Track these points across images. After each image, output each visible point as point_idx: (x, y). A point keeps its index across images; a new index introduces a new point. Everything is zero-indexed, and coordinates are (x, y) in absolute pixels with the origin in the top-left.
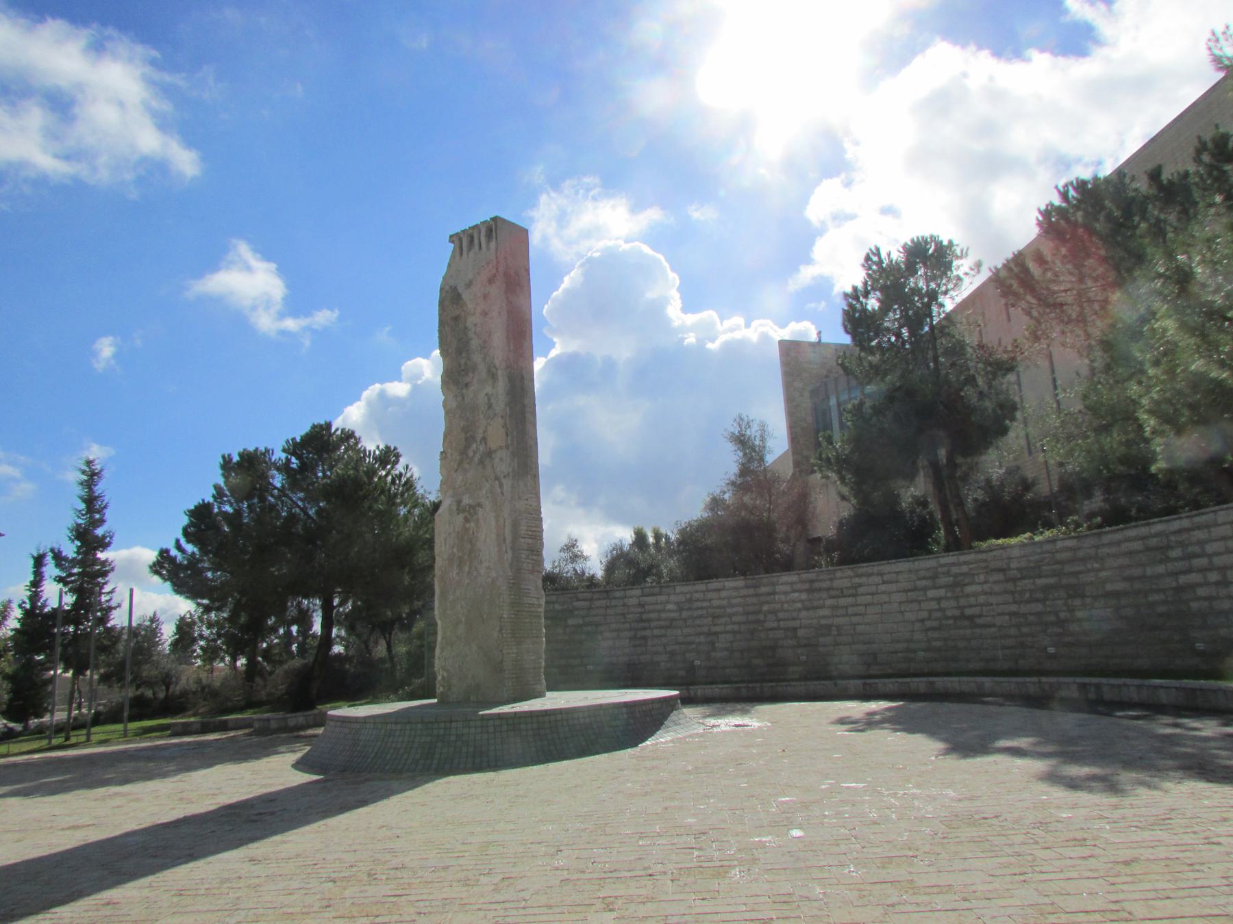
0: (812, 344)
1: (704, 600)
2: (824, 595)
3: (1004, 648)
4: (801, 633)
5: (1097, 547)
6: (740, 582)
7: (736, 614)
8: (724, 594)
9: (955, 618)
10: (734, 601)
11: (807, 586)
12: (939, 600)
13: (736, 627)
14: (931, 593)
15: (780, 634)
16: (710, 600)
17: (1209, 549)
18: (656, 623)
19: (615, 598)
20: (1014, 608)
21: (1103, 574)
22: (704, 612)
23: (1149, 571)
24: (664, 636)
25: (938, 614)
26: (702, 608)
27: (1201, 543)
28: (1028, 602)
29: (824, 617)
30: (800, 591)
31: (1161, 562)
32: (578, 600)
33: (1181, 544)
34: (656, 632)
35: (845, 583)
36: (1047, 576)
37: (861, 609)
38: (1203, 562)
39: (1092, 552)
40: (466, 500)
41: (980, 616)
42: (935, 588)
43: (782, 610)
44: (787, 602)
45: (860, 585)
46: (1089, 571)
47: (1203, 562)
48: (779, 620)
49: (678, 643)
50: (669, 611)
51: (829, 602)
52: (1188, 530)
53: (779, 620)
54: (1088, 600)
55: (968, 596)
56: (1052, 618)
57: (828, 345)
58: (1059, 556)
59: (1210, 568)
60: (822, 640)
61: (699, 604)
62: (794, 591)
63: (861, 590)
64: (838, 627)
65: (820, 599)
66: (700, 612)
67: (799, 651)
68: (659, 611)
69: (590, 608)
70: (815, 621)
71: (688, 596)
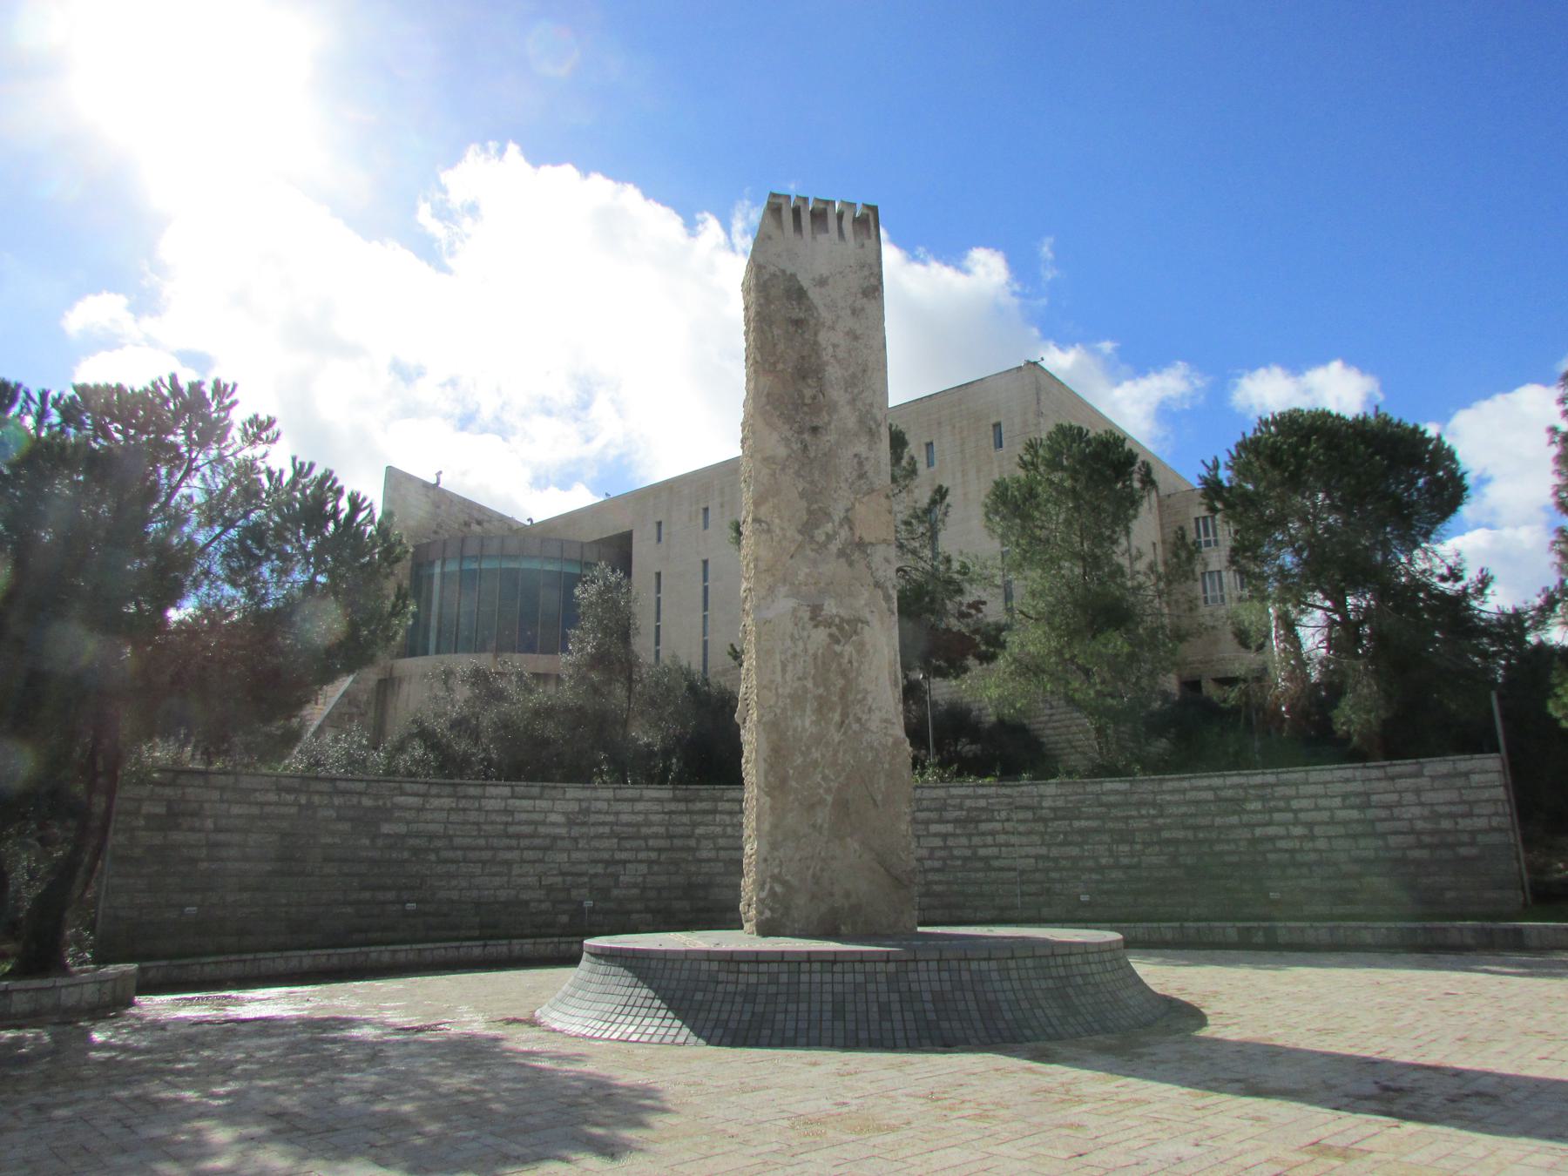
0: (426, 485)
1: (607, 813)
3: (1023, 894)
7: (656, 836)
8: (640, 806)
9: (965, 859)
10: (654, 818)
12: (945, 836)
13: (653, 855)
14: (934, 828)
16: (617, 813)
17: (1295, 804)
19: (465, 797)
20: (1043, 851)
21: (1160, 821)
22: (607, 830)
23: (1218, 821)
24: (541, 861)
25: (943, 853)
26: (603, 824)
27: (1287, 799)
28: (1062, 844)
31: (1234, 812)
32: (404, 793)
33: (1262, 798)
36: (1088, 819)
39: (1150, 797)
40: (830, 608)
41: (997, 858)
42: (941, 821)
46: (1142, 817)
48: (719, 849)
50: (553, 824)
52: (1273, 786)
54: (1138, 847)
55: (983, 834)
56: (1090, 863)
57: (444, 492)
58: (1104, 799)
59: (1296, 822)
61: (602, 818)
66: (601, 830)
71: (584, 805)
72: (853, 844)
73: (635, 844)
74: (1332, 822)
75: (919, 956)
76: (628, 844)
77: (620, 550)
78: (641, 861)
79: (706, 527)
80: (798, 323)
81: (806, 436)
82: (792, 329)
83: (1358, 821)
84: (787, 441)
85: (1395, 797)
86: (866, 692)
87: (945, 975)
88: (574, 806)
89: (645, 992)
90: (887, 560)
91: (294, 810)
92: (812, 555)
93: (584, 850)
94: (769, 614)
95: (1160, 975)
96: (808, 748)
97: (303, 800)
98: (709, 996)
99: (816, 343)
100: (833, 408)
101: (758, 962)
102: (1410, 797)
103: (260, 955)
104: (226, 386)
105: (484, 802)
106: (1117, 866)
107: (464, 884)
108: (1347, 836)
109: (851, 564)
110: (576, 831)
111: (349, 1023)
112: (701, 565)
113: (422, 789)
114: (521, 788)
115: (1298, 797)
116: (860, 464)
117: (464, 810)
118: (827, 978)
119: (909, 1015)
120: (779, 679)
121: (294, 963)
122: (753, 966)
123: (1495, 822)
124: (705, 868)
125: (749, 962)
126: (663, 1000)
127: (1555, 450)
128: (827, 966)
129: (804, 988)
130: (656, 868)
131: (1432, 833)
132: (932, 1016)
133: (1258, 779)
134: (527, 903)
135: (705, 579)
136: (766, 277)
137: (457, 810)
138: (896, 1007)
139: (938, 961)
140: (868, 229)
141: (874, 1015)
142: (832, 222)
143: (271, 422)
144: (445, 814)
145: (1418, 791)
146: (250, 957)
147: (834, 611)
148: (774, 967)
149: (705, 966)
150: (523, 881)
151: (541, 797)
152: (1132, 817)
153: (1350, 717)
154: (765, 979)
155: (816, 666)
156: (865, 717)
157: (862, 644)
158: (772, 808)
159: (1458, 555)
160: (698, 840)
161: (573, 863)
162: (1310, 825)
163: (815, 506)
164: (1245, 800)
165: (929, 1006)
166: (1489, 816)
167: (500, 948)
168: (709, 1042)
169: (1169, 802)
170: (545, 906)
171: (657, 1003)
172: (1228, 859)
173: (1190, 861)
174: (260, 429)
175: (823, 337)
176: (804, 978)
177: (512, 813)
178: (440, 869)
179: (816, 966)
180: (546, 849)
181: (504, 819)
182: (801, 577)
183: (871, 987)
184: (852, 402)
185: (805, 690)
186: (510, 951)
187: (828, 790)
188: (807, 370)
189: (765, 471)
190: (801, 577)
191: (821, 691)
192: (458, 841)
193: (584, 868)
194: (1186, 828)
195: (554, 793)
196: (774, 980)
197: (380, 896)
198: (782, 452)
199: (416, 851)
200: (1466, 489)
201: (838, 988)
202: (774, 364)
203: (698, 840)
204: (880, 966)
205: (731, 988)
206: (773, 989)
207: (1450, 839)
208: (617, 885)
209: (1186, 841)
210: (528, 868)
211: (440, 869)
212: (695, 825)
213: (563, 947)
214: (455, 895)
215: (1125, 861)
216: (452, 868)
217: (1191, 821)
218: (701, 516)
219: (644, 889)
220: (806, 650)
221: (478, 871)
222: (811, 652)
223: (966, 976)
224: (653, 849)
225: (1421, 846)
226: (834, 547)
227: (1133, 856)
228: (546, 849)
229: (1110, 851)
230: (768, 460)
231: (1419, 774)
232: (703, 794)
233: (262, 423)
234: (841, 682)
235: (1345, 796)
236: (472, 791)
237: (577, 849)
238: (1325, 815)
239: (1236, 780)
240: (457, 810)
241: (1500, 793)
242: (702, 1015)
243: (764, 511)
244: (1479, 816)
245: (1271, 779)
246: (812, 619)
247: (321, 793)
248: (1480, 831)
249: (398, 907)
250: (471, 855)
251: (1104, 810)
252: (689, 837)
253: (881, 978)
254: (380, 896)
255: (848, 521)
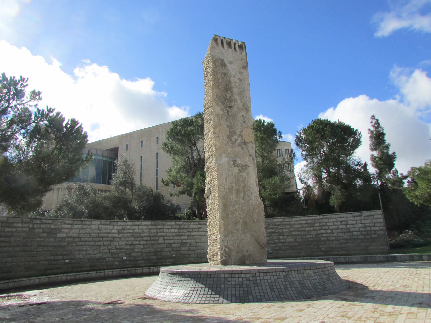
2: (185, 231)
4: (174, 245)
5: (290, 222)
6: (148, 223)
7: (146, 236)
10: (145, 231)
11: (178, 227)
13: (145, 242)
15: (165, 246)
16: (134, 229)
17: (328, 224)
18: (105, 239)
19: (86, 225)
22: (130, 235)
23: (307, 229)
26: (129, 233)
27: (326, 223)
29: (185, 239)
30: (175, 229)
31: (312, 227)
32: (65, 224)
33: (319, 223)
34: (106, 243)
35: (194, 227)
36: (271, 229)
37: (200, 237)
38: (326, 227)
39: (289, 223)
40: (239, 161)
43: (166, 236)
44: (169, 233)
45: (200, 228)
46: (286, 228)
47: (326, 227)
49: (116, 249)
50: (114, 233)
51: (187, 234)
52: (322, 219)
53: (164, 240)
54: (285, 237)
56: (272, 242)
59: (328, 229)
60: (183, 248)
61: (129, 231)
62: (172, 228)
63: (201, 230)
64: (190, 244)
65: (183, 232)
66: (129, 235)
67: (172, 252)
68: (108, 233)
69: (71, 229)
70: (180, 241)
71: (123, 227)
72: (249, 235)
73: (139, 239)
74: (338, 229)
75: (299, 269)
76: (137, 239)
77: (115, 152)
78: (141, 244)
79: (142, 146)
80: (225, 74)
81: (228, 108)
82: (223, 76)
83: (345, 228)
84: (222, 110)
85: (355, 222)
86: (250, 187)
87: (300, 275)
88: (121, 227)
89: (201, 286)
90: (252, 148)
91: (27, 229)
92: (231, 145)
93: (123, 241)
94: (221, 163)
95: (345, 273)
96: (234, 205)
97: (31, 226)
98: (226, 286)
99: (230, 81)
100: (235, 101)
101: (242, 274)
102: (358, 222)
103: (20, 280)
104: (24, 79)
105: (91, 226)
106: (280, 242)
107: (85, 253)
108: (342, 232)
109: (242, 148)
110: (121, 235)
111: (87, 302)
112: (156, 154)
113: (71, 222)
114: (103, 222)
115: (329, 222)
116: (244, 118)
117: (85, 229)
118: (265, 278)
119: (293, 289)
120: (224, 183)
121: (32, 282)
122: (240, 275)
123: (381, 228)
124: (161, 246)
125: (238, 274)
126: (209, 288)
127: (369, 135)
128: (265, 274)
129: (258, 282)
130: (146, 246)
131: (365, 231)
132: (300, 289)
133: (318, 217)
134: (105, 258)
135: (141, 162)
136: (215, 59)
137: (83, 229)
138: (289, 286)
139: (297, 271)
140: (242, 49)
141: (283, 290)
142: (233, 46)
143: (39, 93)
144: (78, 230)
145: (361, 220)
146: (17, 280)
147: (240, 162)
148: (247, 275)
149: (223, 276)
150: (104, 251)
151: (110, 225)
152: (283, 228)
153: (334, 201)
154: (244, 279)
155: (235, 180)
156: (250, 195)
157: (248, 173)
158: (224, 224)
159: (360, 159)
160: (159, 237)
161: (120, 245)
162: (332, 230)
163: (231, 130)
164: (314, 223)
165: (298, 285)
166: (379, 226)
167: (101, 273)
168: (232, 302)
169: (294, 224)
170: (111, 259)
171: (207, 289)
172: (310, 239)
173: (300, 240)
174: (36, 95)
175: (232, 79)
176: (258, 278)
177: (100, 230)
178: (77, 248)
179: (261, 274)
180: (111, 241)
181: (98, 231)
182: (229, 152)
183: (279, 280)
184: (241, 99)
185: (233, 186)
186: (105, 274)
187: (241, 218)
188: (228, 88)
189: (216, 118)
190: (229, 152)
191: (237, 187)
192: (83, 239)
193: (123, 247)
194: (299, 231)
195: (114, 223)
196: (248, 279)
197: (57, 258)
198: (221, 113)
199: (69, 243)
200: (361, 142)
201: (270, 281)
202: (218, 86)
203: (159, 237)
204: (281, 273)
205: (233, 283)
206: (248, 282)
207: (369, 233)
208: (133, 252)
209: (299, 235)
210: (105, 247)
211: (77, 248)
212: (157, 233)
213: (122, 272)
214: (81, 257)
215: (282, 241)
216: (81, 248)
217: (300, 229)
218: (140, 143)
219: (142, 253)
220: (232, 174)
221: (89, 249)
222: (234, 175)
223: (305, 275)
224: (145, 241)
225: (362, 235)
226: (238, 143)
227: (284, 239)
228: (111, 241)
229: (278, 238)
230: (217, 115)
231: (361, 216)
232: (160, 223)
233: (36, 93)
234: (243, 184)
235: (341, 222)
236: (87, 223)
237: (121, 241)
238: (336, 227)
239: (312, 218)
240: (83, 229)
241: (382, 220)
242: (226, 292)
243: (217, 131)
244: (377, 226)
245: (321, 217)
246: (233, 165)
247: (37, 224)
248: (378, 230)
249: (63, 261)
250: (87, 243)
251: (276, 226)
252: (156, 236)
253: (282, 277)
254: (57, 258)
255: (241, 135)
